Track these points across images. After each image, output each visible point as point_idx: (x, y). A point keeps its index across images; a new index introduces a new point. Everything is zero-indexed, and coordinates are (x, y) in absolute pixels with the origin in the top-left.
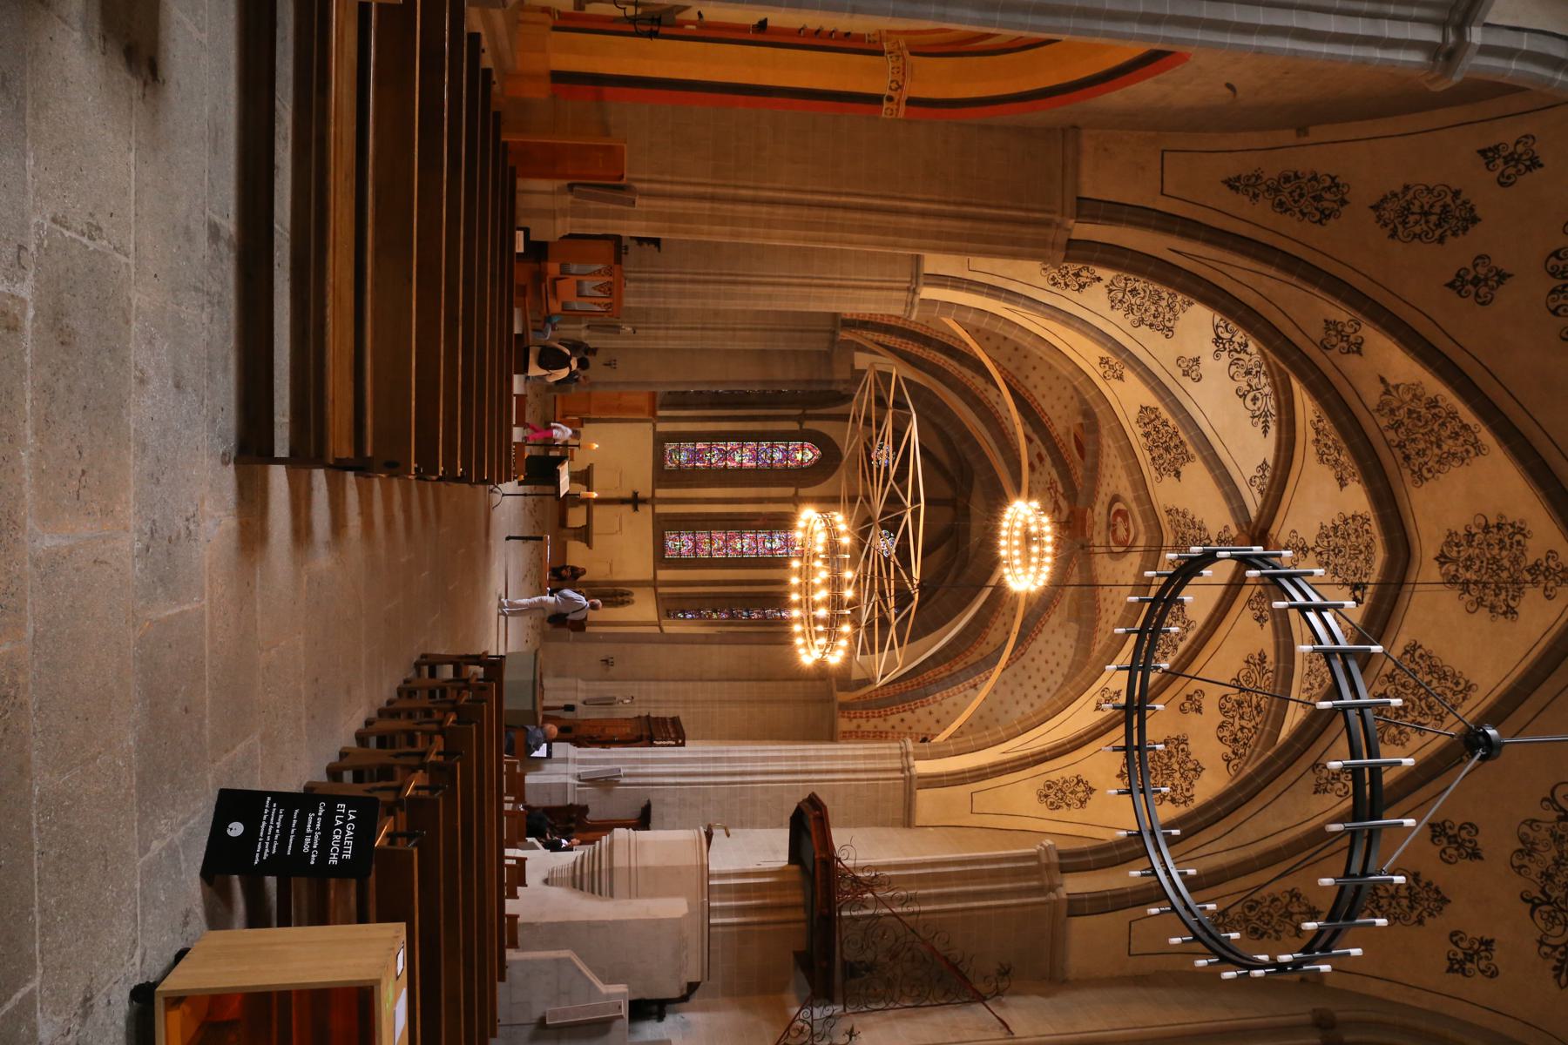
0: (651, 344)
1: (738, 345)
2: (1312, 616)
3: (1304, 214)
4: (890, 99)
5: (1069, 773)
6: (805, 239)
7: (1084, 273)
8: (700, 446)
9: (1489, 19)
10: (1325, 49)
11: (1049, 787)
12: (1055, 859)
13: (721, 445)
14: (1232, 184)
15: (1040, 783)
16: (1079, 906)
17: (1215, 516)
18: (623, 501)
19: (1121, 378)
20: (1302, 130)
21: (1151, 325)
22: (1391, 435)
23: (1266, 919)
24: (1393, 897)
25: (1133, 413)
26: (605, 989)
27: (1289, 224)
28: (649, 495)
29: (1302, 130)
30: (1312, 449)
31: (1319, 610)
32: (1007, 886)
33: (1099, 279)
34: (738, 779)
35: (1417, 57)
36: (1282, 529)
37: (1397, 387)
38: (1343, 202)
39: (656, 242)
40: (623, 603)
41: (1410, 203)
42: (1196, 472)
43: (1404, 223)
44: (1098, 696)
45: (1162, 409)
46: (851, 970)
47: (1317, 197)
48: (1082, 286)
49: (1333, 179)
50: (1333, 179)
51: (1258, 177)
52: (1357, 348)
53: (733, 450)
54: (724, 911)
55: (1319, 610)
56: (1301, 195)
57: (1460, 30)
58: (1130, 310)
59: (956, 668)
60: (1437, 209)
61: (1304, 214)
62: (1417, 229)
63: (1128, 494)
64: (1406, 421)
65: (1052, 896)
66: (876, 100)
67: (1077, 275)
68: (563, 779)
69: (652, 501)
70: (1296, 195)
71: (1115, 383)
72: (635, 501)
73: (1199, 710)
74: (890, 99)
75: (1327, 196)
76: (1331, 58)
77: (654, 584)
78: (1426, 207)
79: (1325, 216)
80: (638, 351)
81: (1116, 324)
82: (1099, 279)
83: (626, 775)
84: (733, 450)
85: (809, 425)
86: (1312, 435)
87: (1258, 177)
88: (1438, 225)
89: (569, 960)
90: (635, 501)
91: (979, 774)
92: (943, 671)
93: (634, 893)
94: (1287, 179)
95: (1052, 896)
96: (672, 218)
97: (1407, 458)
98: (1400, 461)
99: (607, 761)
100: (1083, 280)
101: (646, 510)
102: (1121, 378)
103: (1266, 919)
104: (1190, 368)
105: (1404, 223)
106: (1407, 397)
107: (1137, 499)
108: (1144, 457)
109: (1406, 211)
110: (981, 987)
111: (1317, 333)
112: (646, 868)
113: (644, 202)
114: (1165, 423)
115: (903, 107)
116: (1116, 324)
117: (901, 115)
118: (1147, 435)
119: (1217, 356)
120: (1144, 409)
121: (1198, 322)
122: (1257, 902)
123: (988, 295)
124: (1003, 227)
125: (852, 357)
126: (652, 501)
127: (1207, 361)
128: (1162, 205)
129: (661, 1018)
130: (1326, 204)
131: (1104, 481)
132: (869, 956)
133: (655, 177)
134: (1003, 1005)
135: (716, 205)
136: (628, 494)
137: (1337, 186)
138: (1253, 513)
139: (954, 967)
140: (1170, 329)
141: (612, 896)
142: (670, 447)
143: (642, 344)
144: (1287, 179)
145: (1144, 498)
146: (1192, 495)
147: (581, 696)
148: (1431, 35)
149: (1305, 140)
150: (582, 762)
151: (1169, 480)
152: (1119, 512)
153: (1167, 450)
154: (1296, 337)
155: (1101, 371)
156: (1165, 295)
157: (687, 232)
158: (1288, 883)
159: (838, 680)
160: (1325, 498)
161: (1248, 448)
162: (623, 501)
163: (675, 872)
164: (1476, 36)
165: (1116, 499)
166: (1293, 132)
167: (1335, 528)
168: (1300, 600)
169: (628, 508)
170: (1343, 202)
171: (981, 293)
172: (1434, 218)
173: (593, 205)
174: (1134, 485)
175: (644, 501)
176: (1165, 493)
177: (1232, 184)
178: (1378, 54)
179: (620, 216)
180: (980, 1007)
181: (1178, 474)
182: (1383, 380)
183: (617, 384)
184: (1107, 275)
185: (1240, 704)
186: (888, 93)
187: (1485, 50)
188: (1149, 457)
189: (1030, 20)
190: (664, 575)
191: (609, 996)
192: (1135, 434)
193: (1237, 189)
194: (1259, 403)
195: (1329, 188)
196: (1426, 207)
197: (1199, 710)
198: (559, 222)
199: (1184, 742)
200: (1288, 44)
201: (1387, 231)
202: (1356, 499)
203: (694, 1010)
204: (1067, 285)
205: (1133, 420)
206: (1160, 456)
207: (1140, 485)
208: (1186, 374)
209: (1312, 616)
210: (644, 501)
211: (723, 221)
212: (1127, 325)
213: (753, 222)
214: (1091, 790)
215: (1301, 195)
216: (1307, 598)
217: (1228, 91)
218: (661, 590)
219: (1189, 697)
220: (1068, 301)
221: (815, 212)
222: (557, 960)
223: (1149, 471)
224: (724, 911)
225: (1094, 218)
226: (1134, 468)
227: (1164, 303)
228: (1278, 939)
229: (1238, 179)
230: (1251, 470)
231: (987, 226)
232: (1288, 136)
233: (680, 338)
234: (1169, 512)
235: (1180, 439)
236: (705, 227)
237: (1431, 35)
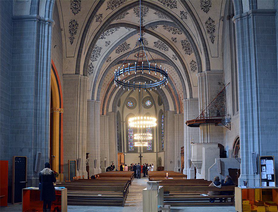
0: (108, 154)
1: (108, 136)
2: (120, 73)
3: (77, 28)
4: (60, 111)
5: (189, 66)
6: (85, 127)
7: (90, 66)
8: (129, 143)
9: (44, 17)
10: (50, 45)
11: (192, 70)
12: (199, 74)
13: (129, 139)
14: (72, 43)
15: (191, 72)
16: (208, 69)
17: (137, 37)
18: (141, 159)
19: (110, 58)
20: (62, 30)
21: (100, 52)
22: (117, 6)
23: (211, 29)
24: (206, 3)
25: (117, 54)
26: (216, 163)
27: (78, 31)
28: (139, 154)
29: (62, 30)
30: (122, 20)
31: (120, 72)
32: (204, 83)
33: (91, 63)
34: (190, 136)
35: (50, 28)
36: (139, 24)
37: (108, 6)
38: (74, 20)
39: (87, 154)
40: (161, 159)
41: (74, 8)
42: (128, 41)
43: (77, 8)
44: (174, 59)
45: (116, 49)
46: (218, 115)
47: (74, 25)
48: (93, 67)
49: (70, 23)
50: (70, 23)
51: (70, 38)
52: (101, 15)
53: (130, 136)
54: (207, 140)
55: (120, 72)
56: (73, 29)
57: (46, 21)
58: (97, 57)
59: (172, 88)
60: (75, 3)
61: (77, 28)
62: (78, 6)
63: (134, 54)
64: (114, 4)
65: (206, 74)
66: (60, 114)
67: (91, 68)
68: (190, 171)
69: (140, 153)
70: (73, 30)
71: (112, 58)
72: (141, 157)
73: (176, 38)
74: (60, 111)
75: (73, 24)
76: (51, 44)
77: (157, 153)
78: (74, 5)
79: (77, 24)
80: (110, 157)
81: (100, 59)
82: (91, 63)
83: (189, 158)
84: (130, 136)
85: (124, 121)
86: (119, 20)
87: (70, 38)
88: (78, 2)
89: (210, 169)
90: (141, 157)
91: (190, 85)
92: (172, 91)
93: (201, 157)
94: (70, 32)
95: (206, 74)
96: (82, 152)
97: (122, 3)
98: (122, 4)
99: (187, 162)
100: (92, 67)
101: (142, 155)
102: (110, 58)
103: (211, 29)
104: (108, 43)
105: (77, 8)
106: (110, 4)
107: (135, 52)
108: (126, 52)
109: (75, 8)
110: (223, 88)
111: (99, 23)
112: (197, 155)
113: (80, 157)
114: (119, 48)
115: (61, 109)
116: (100, 59)
117: (63, 109)
118: (121, 51)
119: (105, 38)
120: (116, 52)
121: (100, 43)
122: (208, 31)
123: (95, 86)
124: (81, 88)
125: (110, 112)
126: (140, 153)
127: (106, 40)
128: (76, 57)
129: (226, 152)
130: (75, 24)
131: (132, 59)
132: (216, 111)
133: (76, 155)
134: (226, 84)
135: (80, 144)
136: (139, 158)
137: (71, 22)
138: (134, 30)
139: (219, 94)
140: (100, 48)
141: (202, 161)
142: (129, 150)
143: (108, 156)
144: (70, 32)
145: (134, 51)
146: (133, 42)
147: (178, 167)
148: (47, 26)
149: (63, 29)
150: (187, 167)
151: (130, 46)
152: (138, 55)
153: (124, 47)
154: (100, 27)
155: (109, 62)
156: (94, 49)
157: (85, 149)
158: (204, 24)
159: (143, 130)
160: (131, 17)
161: (123, 32)
162: (141, 159)
163: (198, 149)
164: (47, 19)
165: (135, 56)
166: (62, 31)
167: (137, 14)
168: (123, 72)
169: (142, 158)
170: (74, 20)
171: (95, 88)
172: (76, 3)
173: (81, 166)
174: (132, 53)
175: (141, 155)
176: (133, 47)
177: (72, 43)
178: (50, 35)
179: (83, 161)
180: (226, 88)
181: (129, 45)
182: (107, 9)
183: (116, 161)
184: (90, 62)
185: (174, 30)
186: (59, 112)
187: (49, 17)
188: (126, 51)
189: (48, 96)
190: (155, 151)
191: (217, 162)
192: (122, 54)
193: (73, 42)
194: (114, 29)
195: (72, 23)
196: (74, 5)
197: (176, 38)
198: (84, 172)
199: (182, 41)
200: (49, 51)
201: (79, 12)
202: (131, 11)
203: (225, 145)
204: (93, 70)
205: (118, 54)
206: (126, 48)
207: (131, 52)
208: (109, 44)
209: (120, 73)
210: (141, 155)
211: (83, 142)
212: (100, 57)
213: (83, 136)
214: (193, 61)
215: (73, 29)
216: (122, 71)
217: (55, 47)
218: (158, 151)
219: (173, 41)
220: (96, 70)
221: (80, 125)
222: (210, 171)
223: (128, 50)
224: (207, 140)
225: (79, 71)
226: (128, 54)
227: (95, 50)
228: (215, 26)
229: (71, 42)
230: (127, 30)
231: (81, 92)
232: (63, 32)
233: (107, 148)
234: (137, 46)
235: (122, 45)
236: (84, 145)
237: (47, 26)
